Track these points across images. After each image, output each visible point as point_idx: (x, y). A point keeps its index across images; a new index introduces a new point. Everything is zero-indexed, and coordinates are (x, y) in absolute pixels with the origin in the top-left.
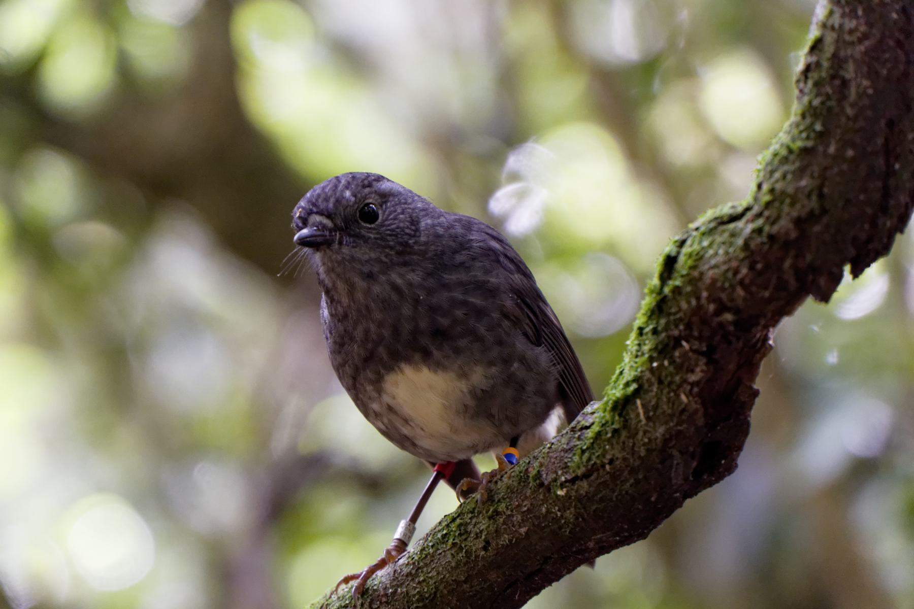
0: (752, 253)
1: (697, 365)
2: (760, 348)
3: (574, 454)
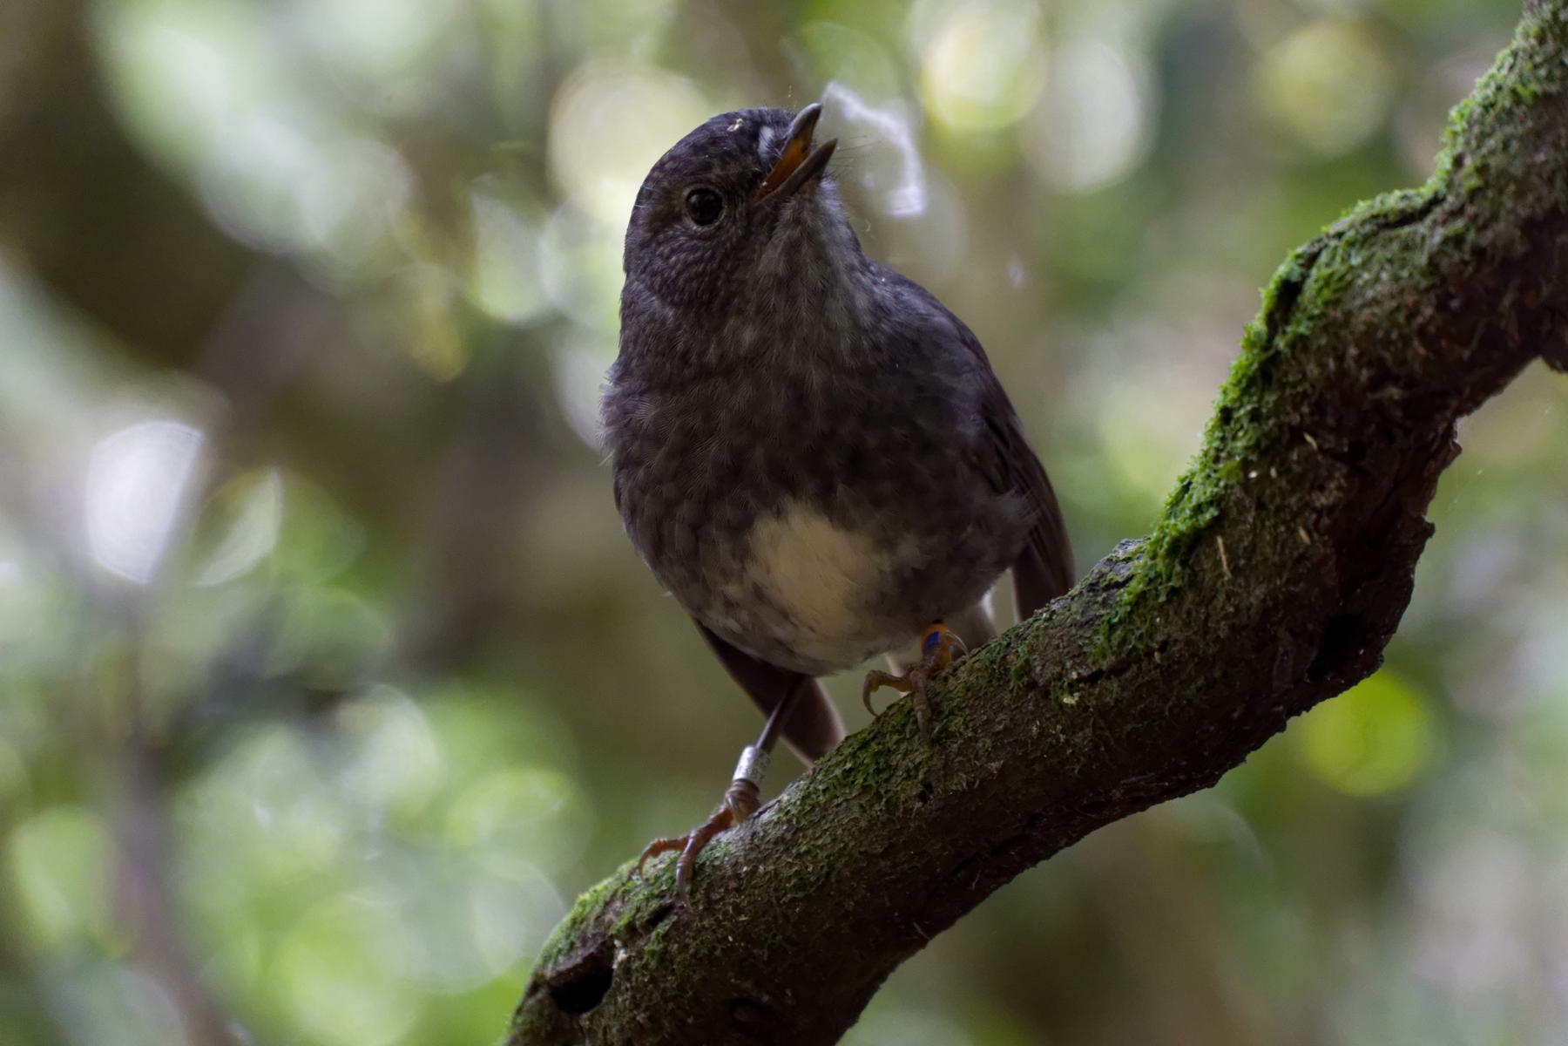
0: (1444, 280)
1: (1330, 477)
3: (1096, 632)
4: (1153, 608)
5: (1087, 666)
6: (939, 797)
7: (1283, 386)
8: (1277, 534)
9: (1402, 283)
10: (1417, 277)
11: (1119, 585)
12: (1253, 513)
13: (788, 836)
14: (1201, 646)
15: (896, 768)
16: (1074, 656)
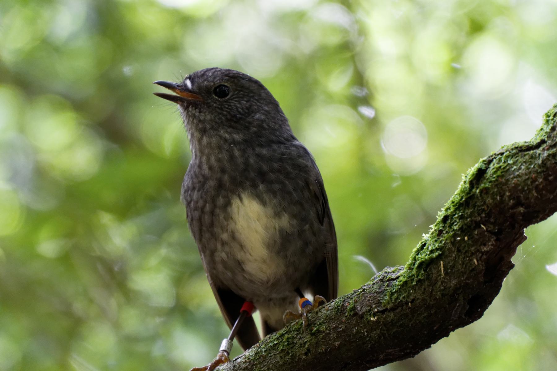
0: (547, 169)
1: (489, 241)
2: (518, 238)
3: (386, 295)
4: (410, 287)
5: (382, 307)
6: (313, 354)
7: (474, 206)
8: (464, 261)
9: (530, 170)
10: (537, 168)
11: (393, 280)
12: (456, 253)
13: (249, 367)
14: (428, 301)
15: (296, 343)
16: (376, 303)
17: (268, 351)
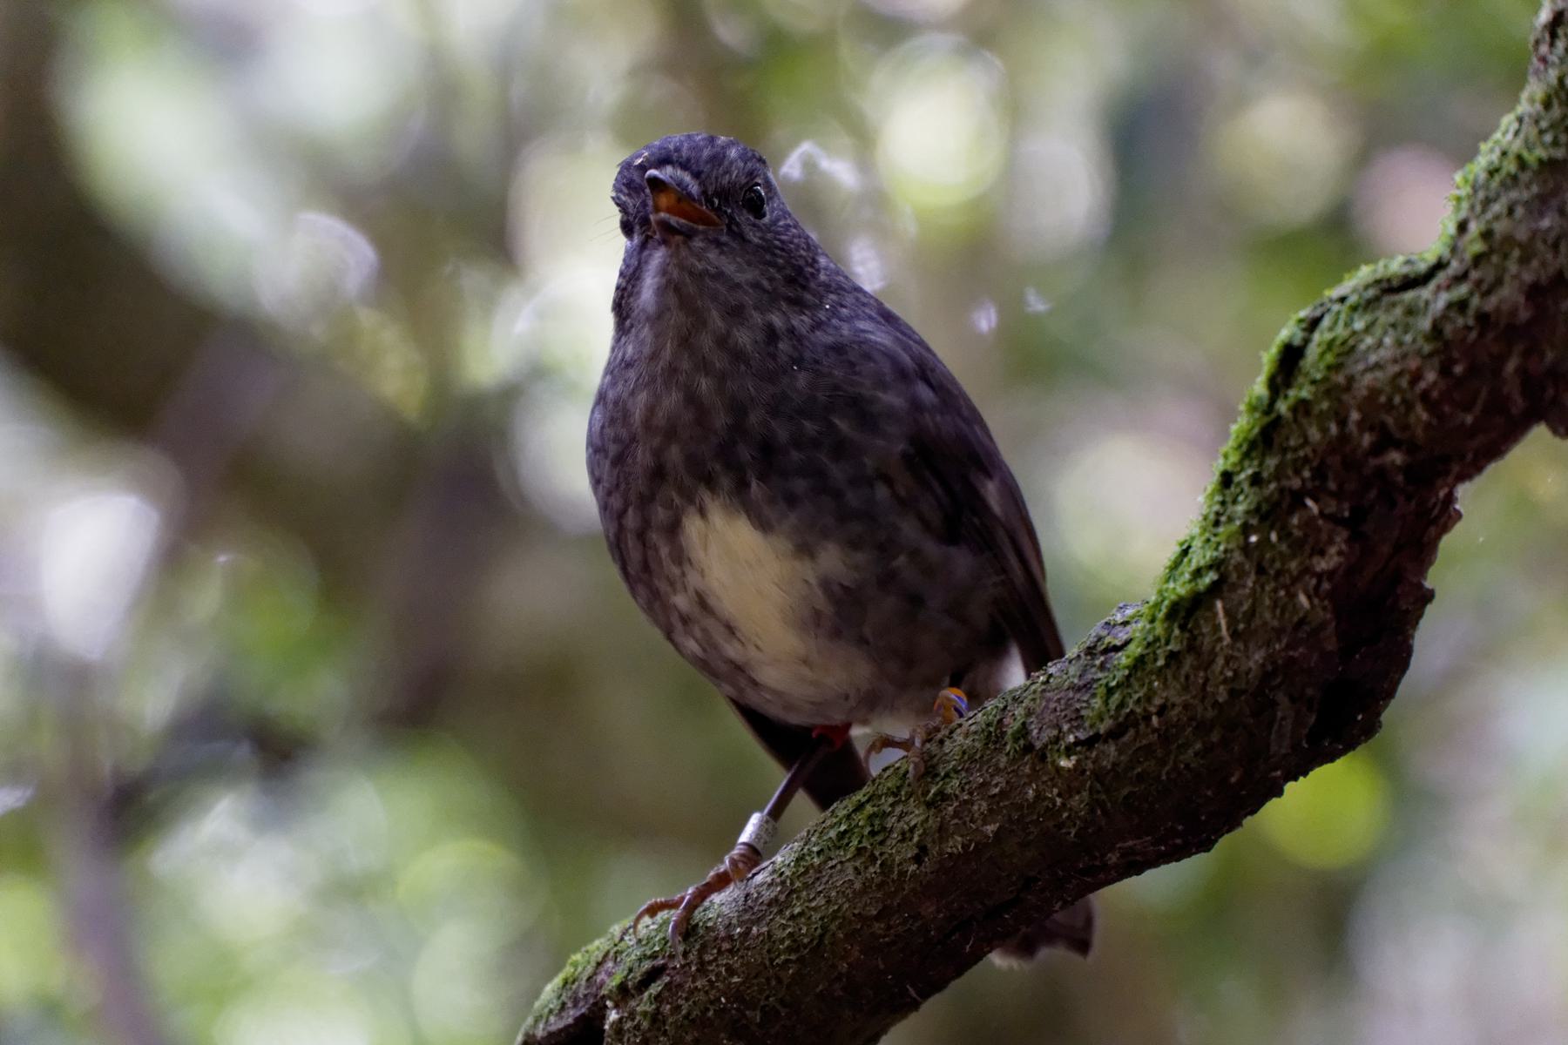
0: (1447, 344)
1: (1331, 542)
3: (1094, 695)
4: (1151, 673)
10: (1420, 341)
11: (1117, 649)
13: (782, 898)
15: (891, 831)
17: (826, 851)
